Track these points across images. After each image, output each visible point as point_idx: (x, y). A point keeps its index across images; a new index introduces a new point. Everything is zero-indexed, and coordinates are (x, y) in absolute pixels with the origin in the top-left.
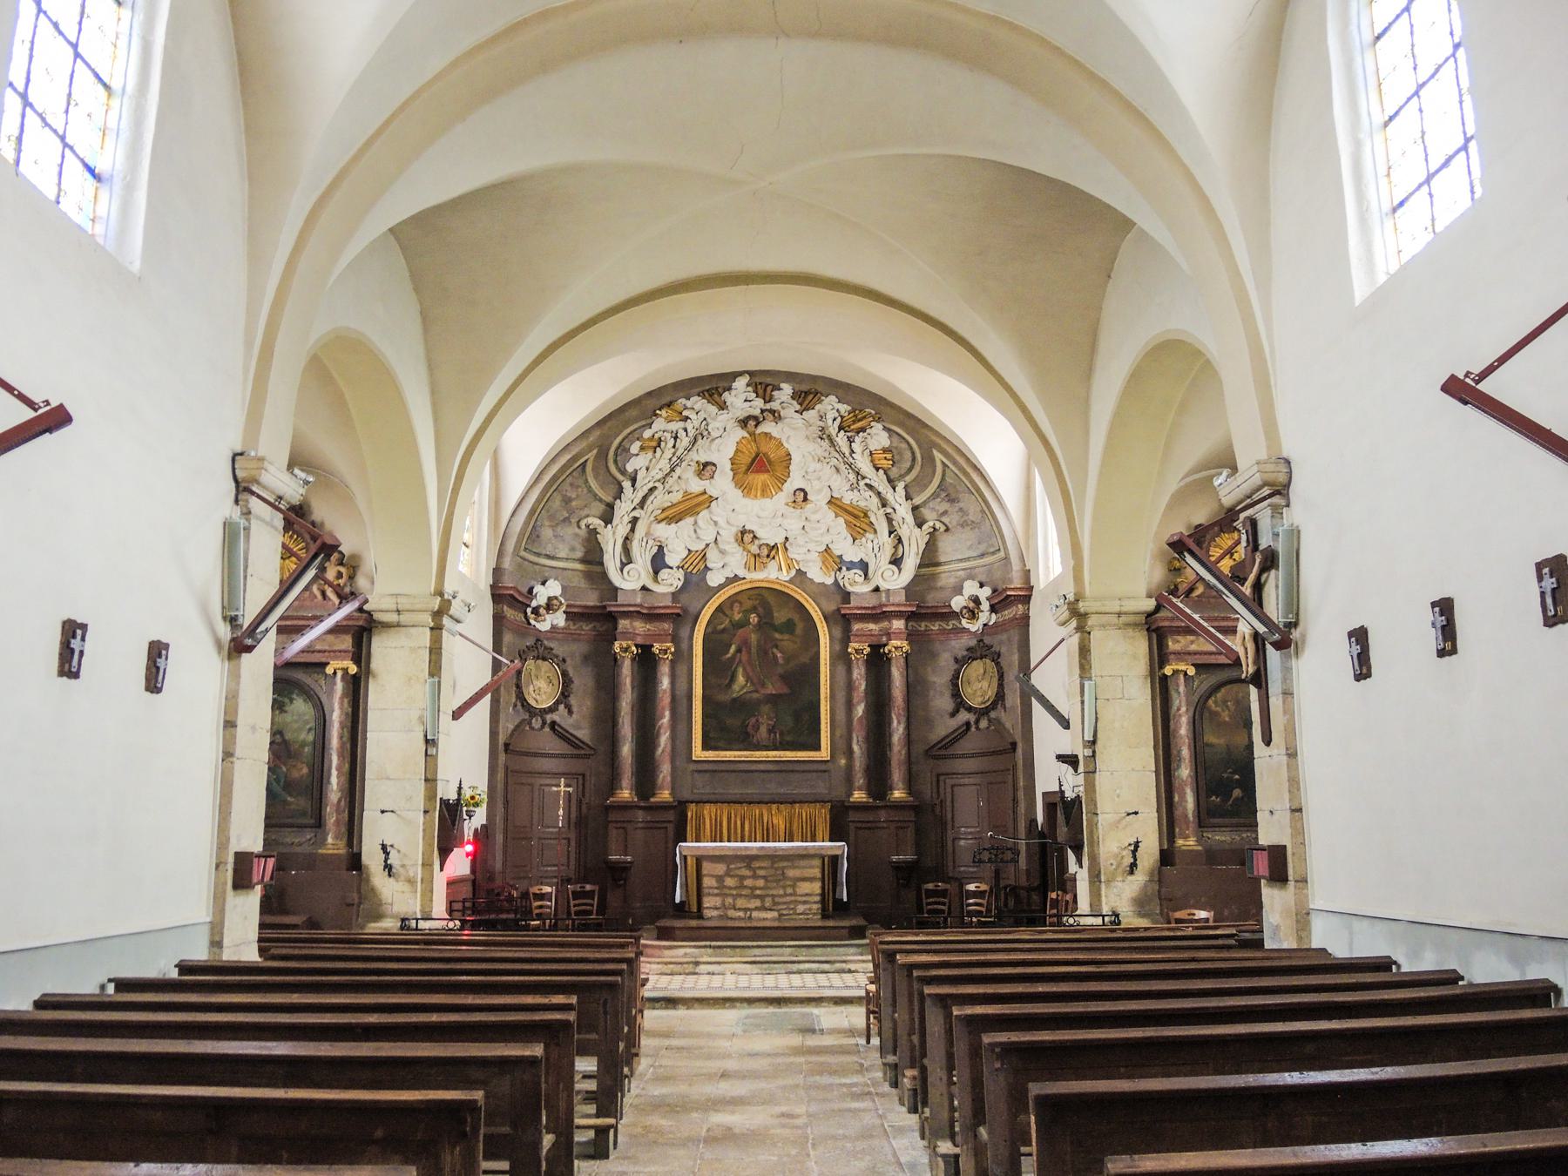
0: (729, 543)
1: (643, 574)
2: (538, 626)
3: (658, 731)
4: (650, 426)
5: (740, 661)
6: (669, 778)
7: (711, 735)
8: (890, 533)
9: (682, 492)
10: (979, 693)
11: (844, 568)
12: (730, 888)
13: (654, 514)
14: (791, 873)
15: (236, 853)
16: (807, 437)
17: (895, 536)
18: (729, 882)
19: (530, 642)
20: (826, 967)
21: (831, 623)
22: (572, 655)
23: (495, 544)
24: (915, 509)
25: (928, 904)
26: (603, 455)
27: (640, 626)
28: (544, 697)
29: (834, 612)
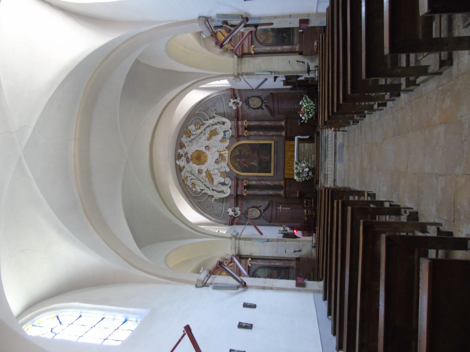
0: (219, 166)
4: (189, 186)
6: (278, 182)
8: (216, 125)
9: (206, 178)
11: (225, 137)
13: (211, 185)
16: (192, 146)
19: (243, 216)
24: (210, 118)
26: (196, 198)
27: (240, 188)
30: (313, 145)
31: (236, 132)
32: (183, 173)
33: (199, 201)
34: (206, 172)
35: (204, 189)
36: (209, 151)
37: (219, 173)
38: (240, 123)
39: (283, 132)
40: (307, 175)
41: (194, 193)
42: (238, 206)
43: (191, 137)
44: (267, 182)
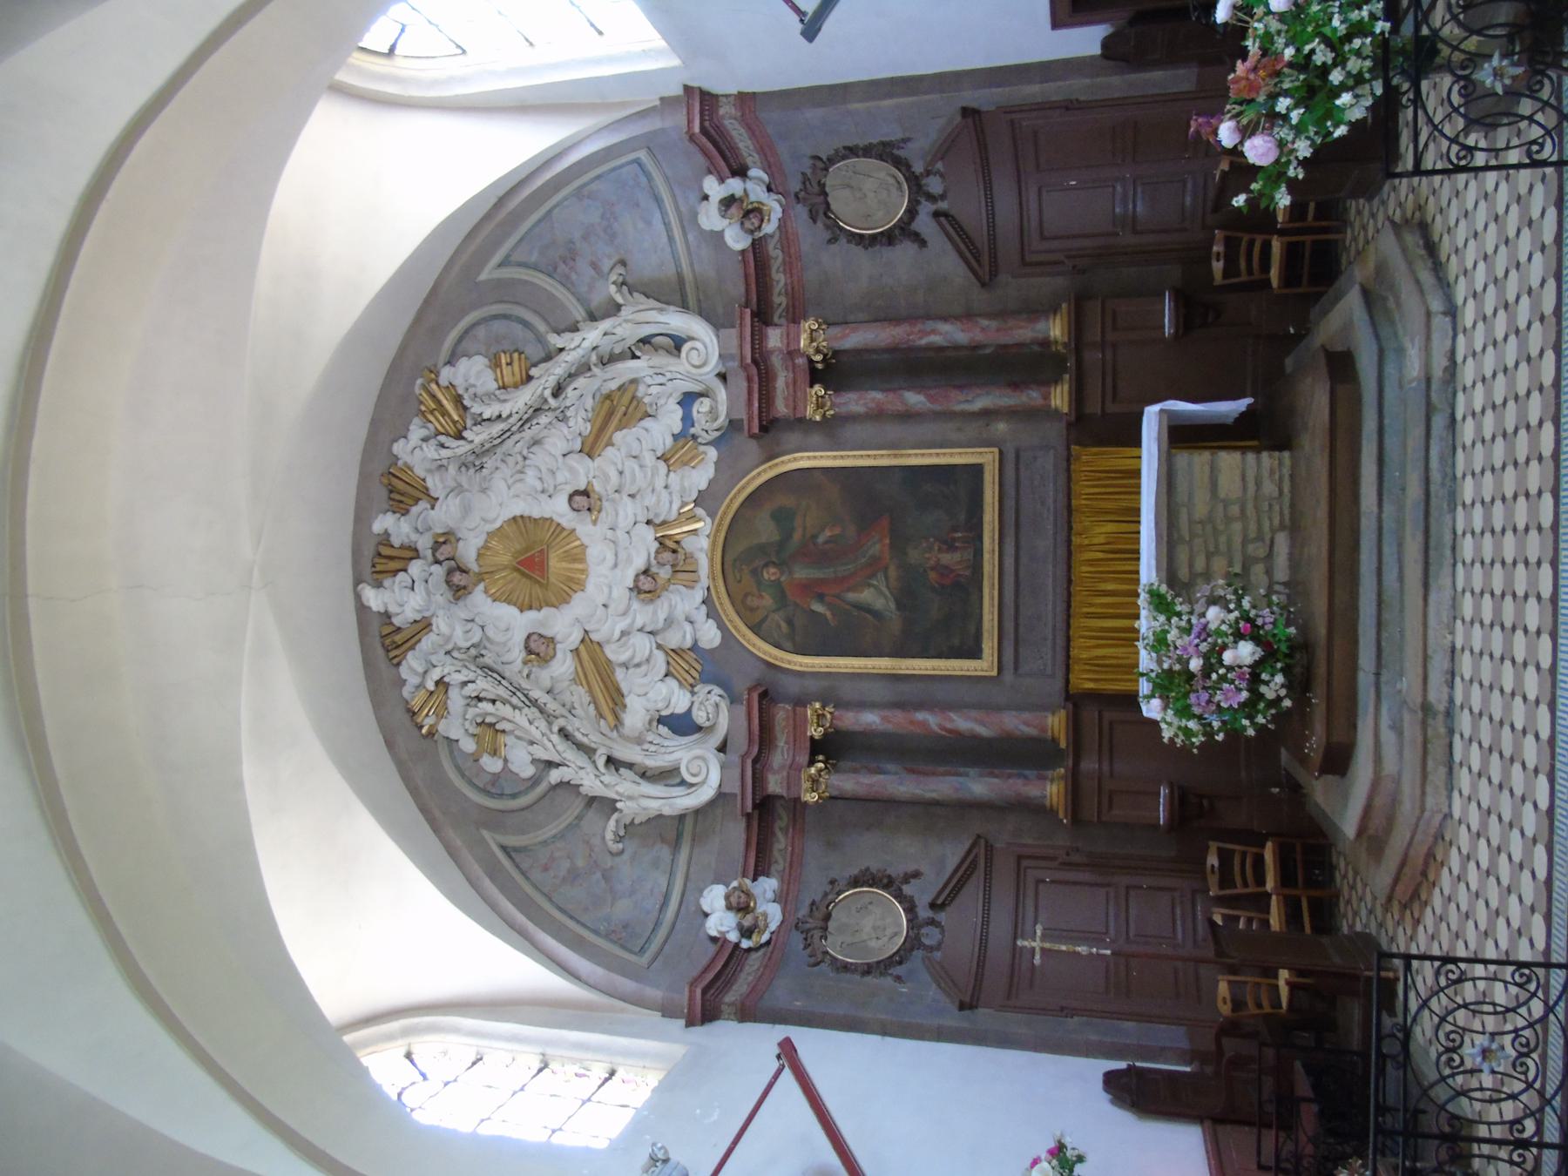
0: (655, 613)
2: (773, 926)
3: (950, 731)
4: (452, 743)
6: (1027, 716)
8: (634, 357)
9: (574, 687)
11: (692, 430)
14: (1201, 510)
15: (1056, 24)
16: (484, 491)
19: (797, 940)
23: (622, 1011)
24: (593, 317)
25: (1250, 271)
26: (495, 821)
27: (780, 757)
30: (1281, 464)
31: (756, 395)
32: (412, 663)
33: (512, 841)
34: (576, 651)
35: (556, 759)
36: (595, 522)
37: (660, 657)
38: (775, 338)
39: (1059, 389)
40: (1245, 695)
41: (484, 791)
42: (774, 868)
43: (466, 434)
44: (952, 715)
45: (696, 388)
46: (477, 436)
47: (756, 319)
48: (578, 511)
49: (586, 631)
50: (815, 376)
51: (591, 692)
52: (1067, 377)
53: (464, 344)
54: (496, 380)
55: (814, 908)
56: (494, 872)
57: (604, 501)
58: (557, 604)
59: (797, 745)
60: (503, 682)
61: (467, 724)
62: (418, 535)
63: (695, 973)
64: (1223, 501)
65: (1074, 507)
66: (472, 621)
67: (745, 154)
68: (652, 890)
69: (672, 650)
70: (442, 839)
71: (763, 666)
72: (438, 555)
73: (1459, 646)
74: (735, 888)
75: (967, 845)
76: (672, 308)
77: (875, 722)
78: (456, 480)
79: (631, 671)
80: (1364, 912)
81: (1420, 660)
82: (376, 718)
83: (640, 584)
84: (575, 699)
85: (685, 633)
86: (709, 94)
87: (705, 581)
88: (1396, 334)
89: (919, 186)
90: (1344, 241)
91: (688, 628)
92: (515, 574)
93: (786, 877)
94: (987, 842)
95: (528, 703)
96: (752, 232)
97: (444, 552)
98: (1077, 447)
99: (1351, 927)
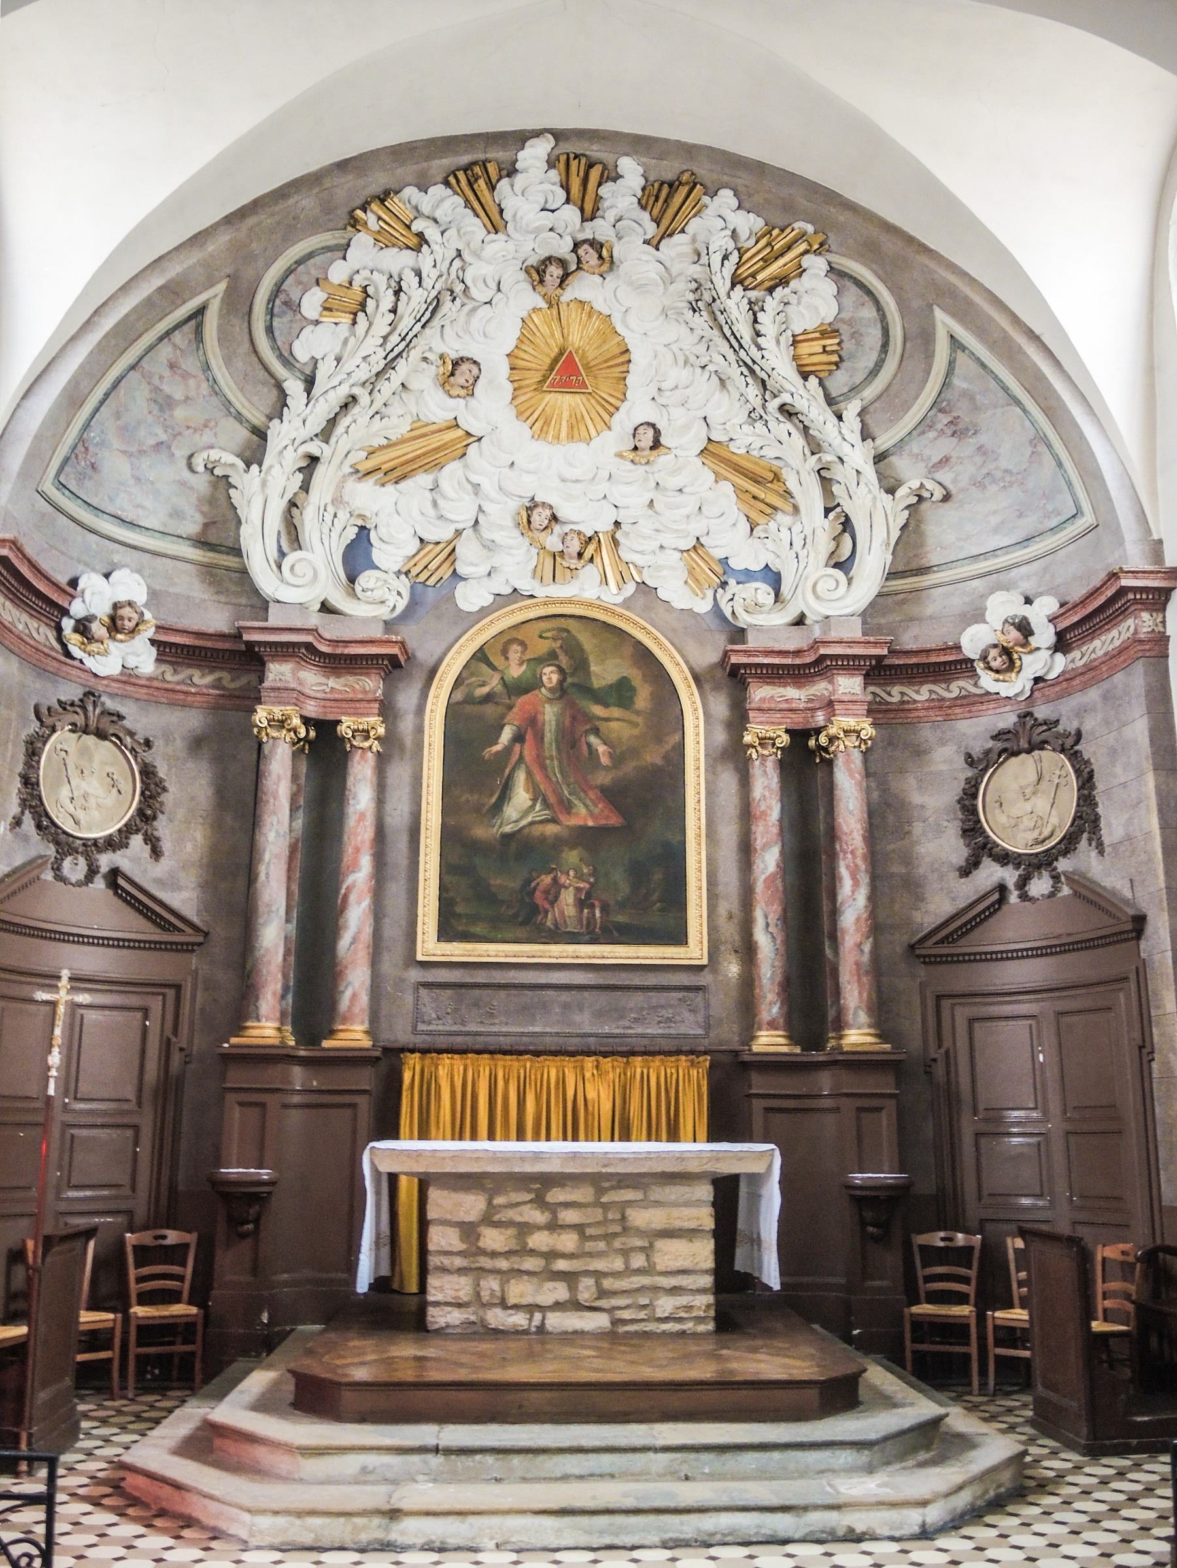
0: (502, 528)
1: (323, 573)
2: (90, 663)
3: (346, 896)
5: (521, 758)
7: (459, 909)
8: (827, 511)
10: (1027, 822)
11: (732, 582)
12: (494, 1254)
13: (351, 459)
14: (640, 1218)
17: (837, 517)
18: (493, 1239)
19: (72, 692)
20: (781, 1524)
21: (707, 687)
22: (168, 737)
24: (880, 458)
25: (929, 1279)
27: (311, 679)
28: (96, 814)
29: (713, 667)
30: (699, 1320)
31: (776, 661)
35: (317, 390)
36: (620, 455)
37: (446, 534)
38: (849, 685)
39: (782, 1041)
41: (277, 290)
45: (785, 589)
46: (736, 305)
47: (874, 662)
48: (634, 436)
49: (480, 439)
50: (800, 736)
51: (402, 441)
52: (798, 1050)
53: (854, 289)
54: (805, 332)
55: (115, 718)
56: (173, 292)
57: (647, 468)
58: (516, 403)
59: (329, 704)
60: (419, 325)
61: (365, 273)
62: (612, 220)
63: (29, 551)
64: (651, 1245)
65: (631, 1058)
66: (499, 290)
67: (1084, 648)
68: (142, 507)
69: (454, 550)
70: (215, 227)
71: (431, 661)
72: (586, 246)
73: (480, 1557)
74: (142, 614)
75: (195, 920)
76: (890, 558)
77: (358, 803)
78: (679, 275)
79: (428, 494)
80: (105, 1431)
81: (458, 1507)
82: (378, 150)
83: (539, 509)
84: (394, 420)
85: (476, 565)
86: (1167, 600)
87: (541, 592)
88: (888, 1463)
89: (1039, 867)
90: (970, 1393)
91: (483, 569)
92: (557, 350)
93: (156, 684)
94: (200, 944)
95: (389, 358)
96: (984, 658)
97: (589, 256)
98: (708, 1064)
99: (86, 1416)
